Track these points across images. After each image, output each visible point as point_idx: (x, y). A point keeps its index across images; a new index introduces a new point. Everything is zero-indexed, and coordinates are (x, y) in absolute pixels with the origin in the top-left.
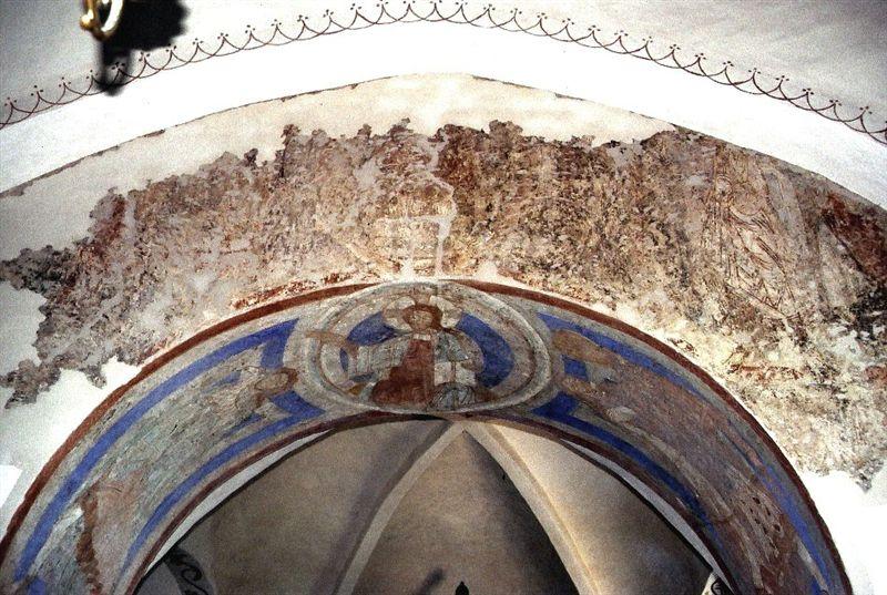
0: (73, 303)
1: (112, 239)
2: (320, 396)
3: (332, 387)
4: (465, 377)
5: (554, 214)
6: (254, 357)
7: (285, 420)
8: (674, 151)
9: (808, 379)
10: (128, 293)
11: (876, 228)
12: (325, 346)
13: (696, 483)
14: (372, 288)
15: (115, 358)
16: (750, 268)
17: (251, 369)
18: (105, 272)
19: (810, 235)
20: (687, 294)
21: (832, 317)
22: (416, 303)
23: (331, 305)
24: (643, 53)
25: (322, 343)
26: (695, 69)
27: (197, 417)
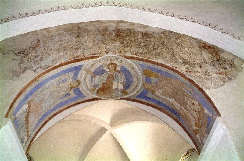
0: (28, 58)
1: (37, 46)
2: (85, 91)
3: (87, 88)
4: (121, 87)
5: (142, 44)
6: (71, 74)
7: (75, 97)
8: (167, 35)
9: (203, 73)
10: (42, 56)
11: (214, 49)
12: (88, 75)
13: (178, 107)
14: (101, 57)
15: (40, 68)
16: (188, 54)
17: (70, 79)
18: (36, 52)
19: (200, 49)
20: (174, 58)
21: (207, 63)
22: (111, 62)
23: (91, 61)
24: (161, 13)
25: (87, 73)
26: (173, 16)
27: (56, 90)
